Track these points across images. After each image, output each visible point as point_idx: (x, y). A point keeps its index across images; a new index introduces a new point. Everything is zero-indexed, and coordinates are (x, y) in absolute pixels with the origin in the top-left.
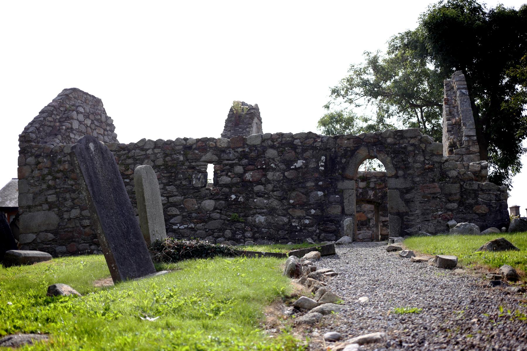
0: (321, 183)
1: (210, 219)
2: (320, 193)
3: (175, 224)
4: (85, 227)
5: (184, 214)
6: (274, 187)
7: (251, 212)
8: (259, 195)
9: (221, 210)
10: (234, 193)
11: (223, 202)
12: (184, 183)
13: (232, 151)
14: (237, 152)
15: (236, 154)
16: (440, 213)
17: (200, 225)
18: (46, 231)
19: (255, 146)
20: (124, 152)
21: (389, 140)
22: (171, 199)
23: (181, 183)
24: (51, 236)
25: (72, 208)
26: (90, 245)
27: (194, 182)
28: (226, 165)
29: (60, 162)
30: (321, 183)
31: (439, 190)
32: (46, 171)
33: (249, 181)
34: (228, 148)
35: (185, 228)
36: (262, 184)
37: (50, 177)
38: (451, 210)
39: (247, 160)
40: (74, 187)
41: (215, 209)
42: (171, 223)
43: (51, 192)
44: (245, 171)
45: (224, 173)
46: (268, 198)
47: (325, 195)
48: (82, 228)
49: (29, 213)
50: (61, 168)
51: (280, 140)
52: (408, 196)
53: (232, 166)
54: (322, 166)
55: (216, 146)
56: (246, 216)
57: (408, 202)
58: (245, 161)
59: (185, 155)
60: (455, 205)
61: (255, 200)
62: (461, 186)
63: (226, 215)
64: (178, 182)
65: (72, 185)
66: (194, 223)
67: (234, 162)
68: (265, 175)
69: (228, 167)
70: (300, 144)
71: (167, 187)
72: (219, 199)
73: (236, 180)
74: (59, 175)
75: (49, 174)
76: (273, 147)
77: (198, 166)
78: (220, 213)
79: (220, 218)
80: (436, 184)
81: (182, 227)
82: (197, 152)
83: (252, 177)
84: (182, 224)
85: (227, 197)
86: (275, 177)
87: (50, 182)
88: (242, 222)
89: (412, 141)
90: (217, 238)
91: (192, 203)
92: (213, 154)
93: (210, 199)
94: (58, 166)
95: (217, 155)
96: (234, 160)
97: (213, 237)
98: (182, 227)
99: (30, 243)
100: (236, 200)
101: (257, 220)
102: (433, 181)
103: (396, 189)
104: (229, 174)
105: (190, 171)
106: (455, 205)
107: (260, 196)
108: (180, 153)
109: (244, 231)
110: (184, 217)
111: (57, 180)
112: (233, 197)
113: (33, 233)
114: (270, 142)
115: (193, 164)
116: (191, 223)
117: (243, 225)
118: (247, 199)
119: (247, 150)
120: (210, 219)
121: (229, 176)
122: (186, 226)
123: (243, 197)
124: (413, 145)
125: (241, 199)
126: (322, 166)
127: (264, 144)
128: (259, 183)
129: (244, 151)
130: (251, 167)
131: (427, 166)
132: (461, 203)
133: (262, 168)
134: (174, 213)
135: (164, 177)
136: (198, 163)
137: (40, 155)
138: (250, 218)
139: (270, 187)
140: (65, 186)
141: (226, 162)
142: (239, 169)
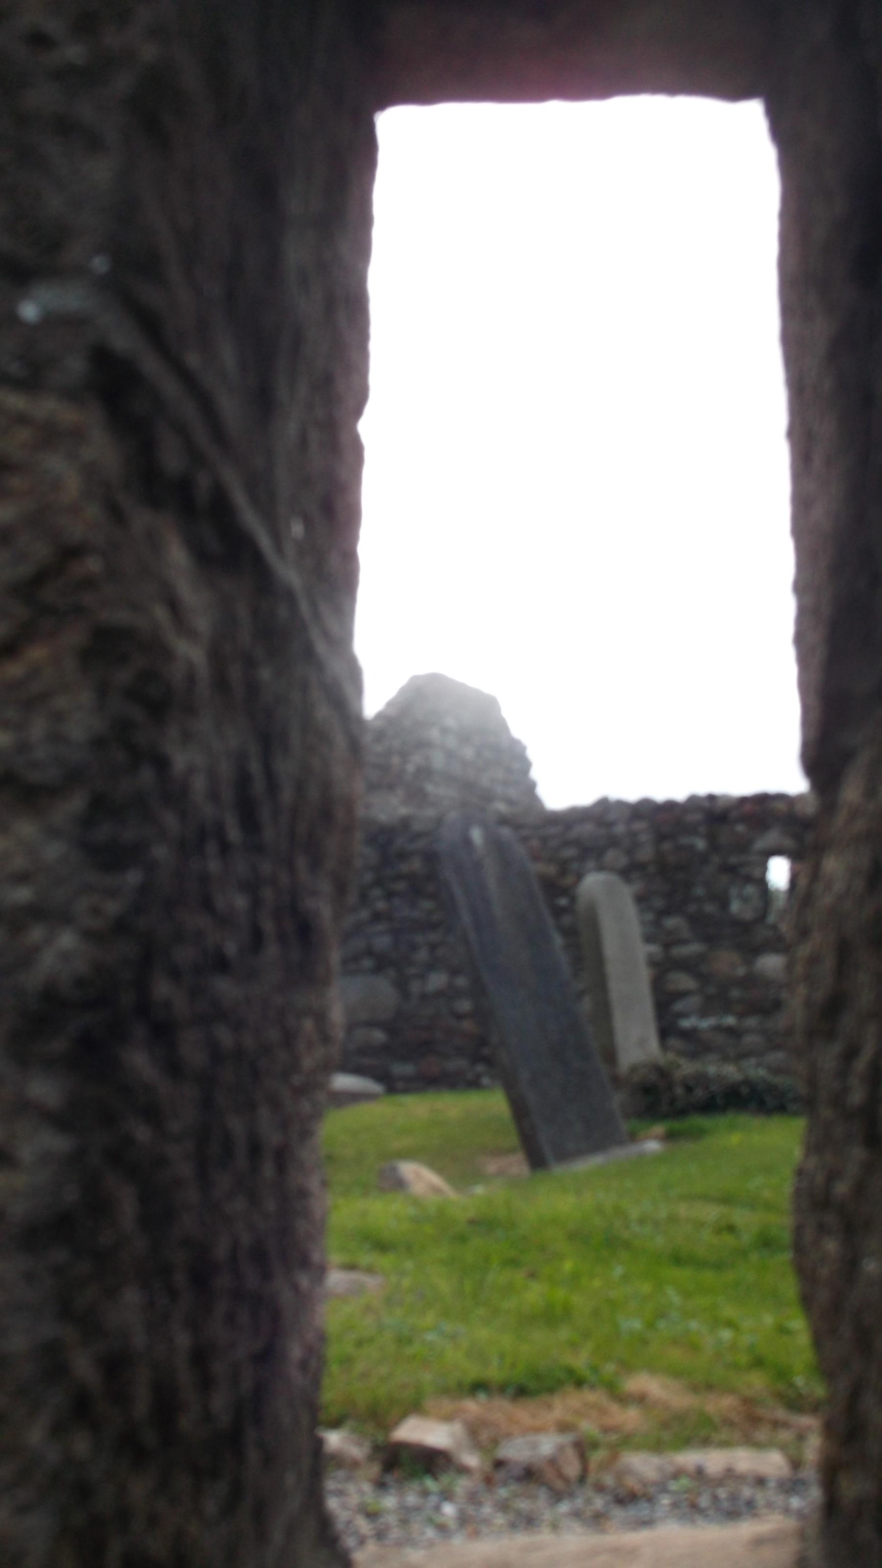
17: (751, 1022)
29: (403, 856)
43: (380, 927)
59: (712, 838)
64: (692, 908)
74: (401, 886)
81: (705, 1024)
84: (703, 1013)
98: (705, 1024)
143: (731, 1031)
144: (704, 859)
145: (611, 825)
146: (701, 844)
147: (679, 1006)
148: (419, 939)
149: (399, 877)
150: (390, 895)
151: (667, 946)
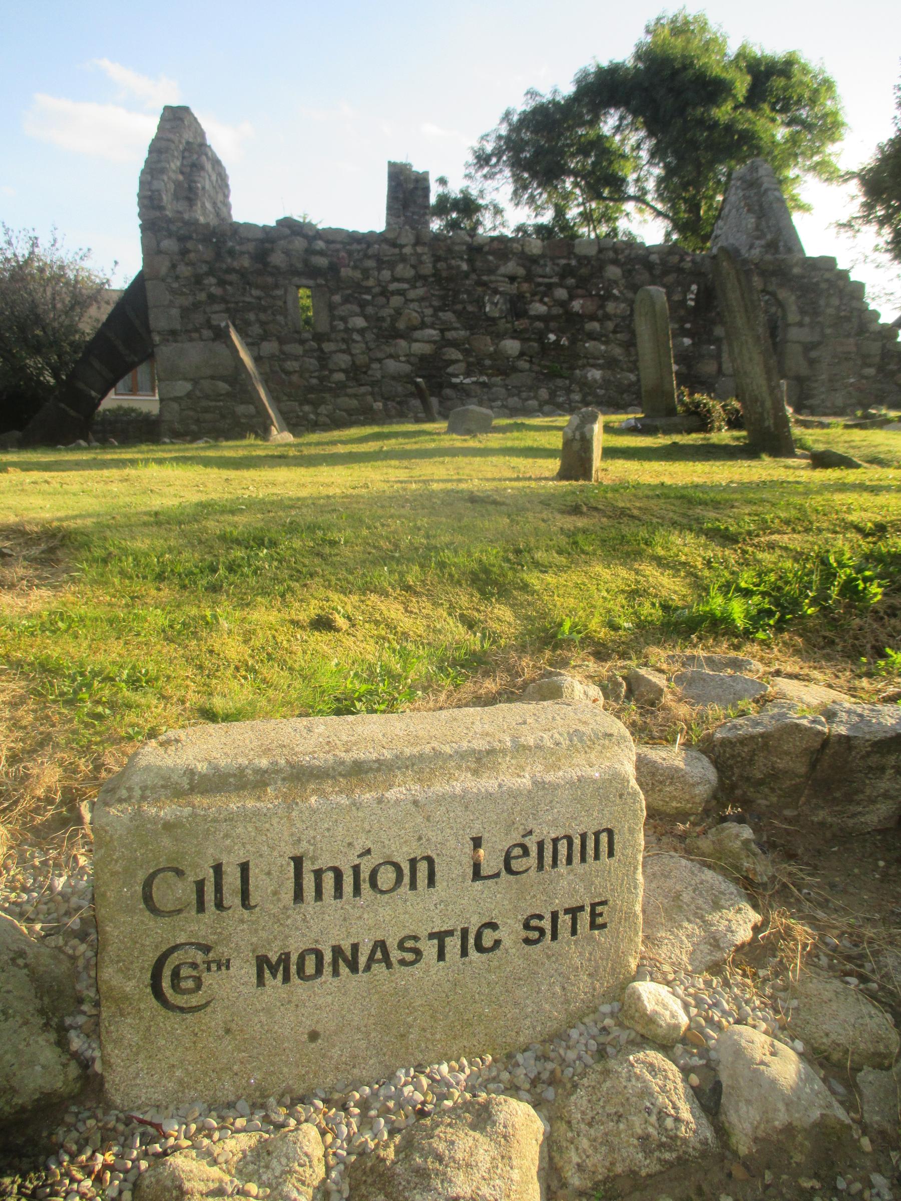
0: (688, 326)
1: (515, 369)
2: (687, 341)
3: (456, 376)
4: (288, 373)
5: (471, 359)
6: (616, 326)
7: (580, 363)
8: (591, 336)
9: (531, 357)
10: (552, 332)
11: (536, 345)
12: (470, 308)
13: (549, 263)
14: (558, 265)
15: (556, 269)
16: (852, 380)
17: (498, 379)
18: (212, 378)
19: (586, 257)
20: (359, 247)
21: (796, 271)
22: (450, 335)
23: (464, 308)
24: (223, 387)
25: (264, 337)
26: (301, 404)
27: (487, 309)
28: (540, 284)
29: (231, 253)
30: (688, 326)
31: (854, 349)
32: (204, 268)
33: (577, 314)
34: (543, 256)
35: (473, 383)
36: (598, 320)
37: (212, 280)
38: (866, 378)
39: (573, 281)
40: (263, 302)
41: (522, 354)
42: (448, 374)
43: (216, 307)
44: (572, 297)
45: (537, 298)
46: (606, 343)
47: (693, 344)
48: (283, 376)
49: (174, 345)
50: (236, 265)
51: (627, 252)
52: (813, 354)
53: (550, 286)
54: (691, 299)
55: (523, 252)
56: (572, 368)
57: (812, 362)
58: (571, 281)
59: (470, 261)
60: (871, 371)
61: (587, 345)
62: (884, 346)
63: (539, 365)
64: (459, 307)
65: (259, 298)
66: (487, 375)
67: (552, 280)
68: (602, 307)
69: (542, 288)
70: (658, 261)
71: (441, 314)
72: (529, 340)
73: (557, 311)
74: (233, 277)
75: (211, 272)
76: (615, 262)
77: (491, 282)
78: (531, 362)
79: (530, 370)
80: (852, 341)
81: (467, 381)
82: (491, 258)
83: (582, 307)
84: (468, 374)
85: (541, 337)
86: (618, 311)
87: (213, 290)
88: (566, 378)
89: (827, 275)
90: (527, 400)
91: (486, 344)
92: (518, 265)
93: (513, 338)
94: (229, 260)
95: (523, 266)
96: (551, 277)
97: (520, 398)
98: (467, 381)
99: (181, 398)
100: (557, 341)
101: (589, 375)
102: (848, 336)
103: (799, 342)
104: (546, 299)
105: (480, 289)
106: (871, 371)
107: (595, 339)
108: (462, 259)
109: (569, 391)
110: (469, 365)
111: (228, 287)
112: (552, 337)
113: (185, 379)
114: (611, 254)
115: (485, 278)
116: (481, 373)
117: (567, 382)
118: (573, 341)
119: (573, 262)
120: (515, 369)
121: (545, 304)
122: (474, 379)
123: (568, 339)
124: (827, 280)
125: (564, 341)
126: (691, 299)
127: (601, 256)
128: (593, 318)
129: (568, 265)
130: (580, 292)
131: (843, 314)
132: (881, 369)
133: (598, 295)
134: (454, 357)
135: (433, 295)
136: (493, 278)
137: (190, 238)
138: (577, 372)
139: (610, 325)
140: (248, 299)
141: (540, 280)
142: (561, 293)
143: (484, 385)
144: (466, 275)
145: (402, 247)
146: (465, 267)
147: (450, 370)
148: (252, 316)
149: (230, 270)
150: (222, 283)
151: (442, 331)
